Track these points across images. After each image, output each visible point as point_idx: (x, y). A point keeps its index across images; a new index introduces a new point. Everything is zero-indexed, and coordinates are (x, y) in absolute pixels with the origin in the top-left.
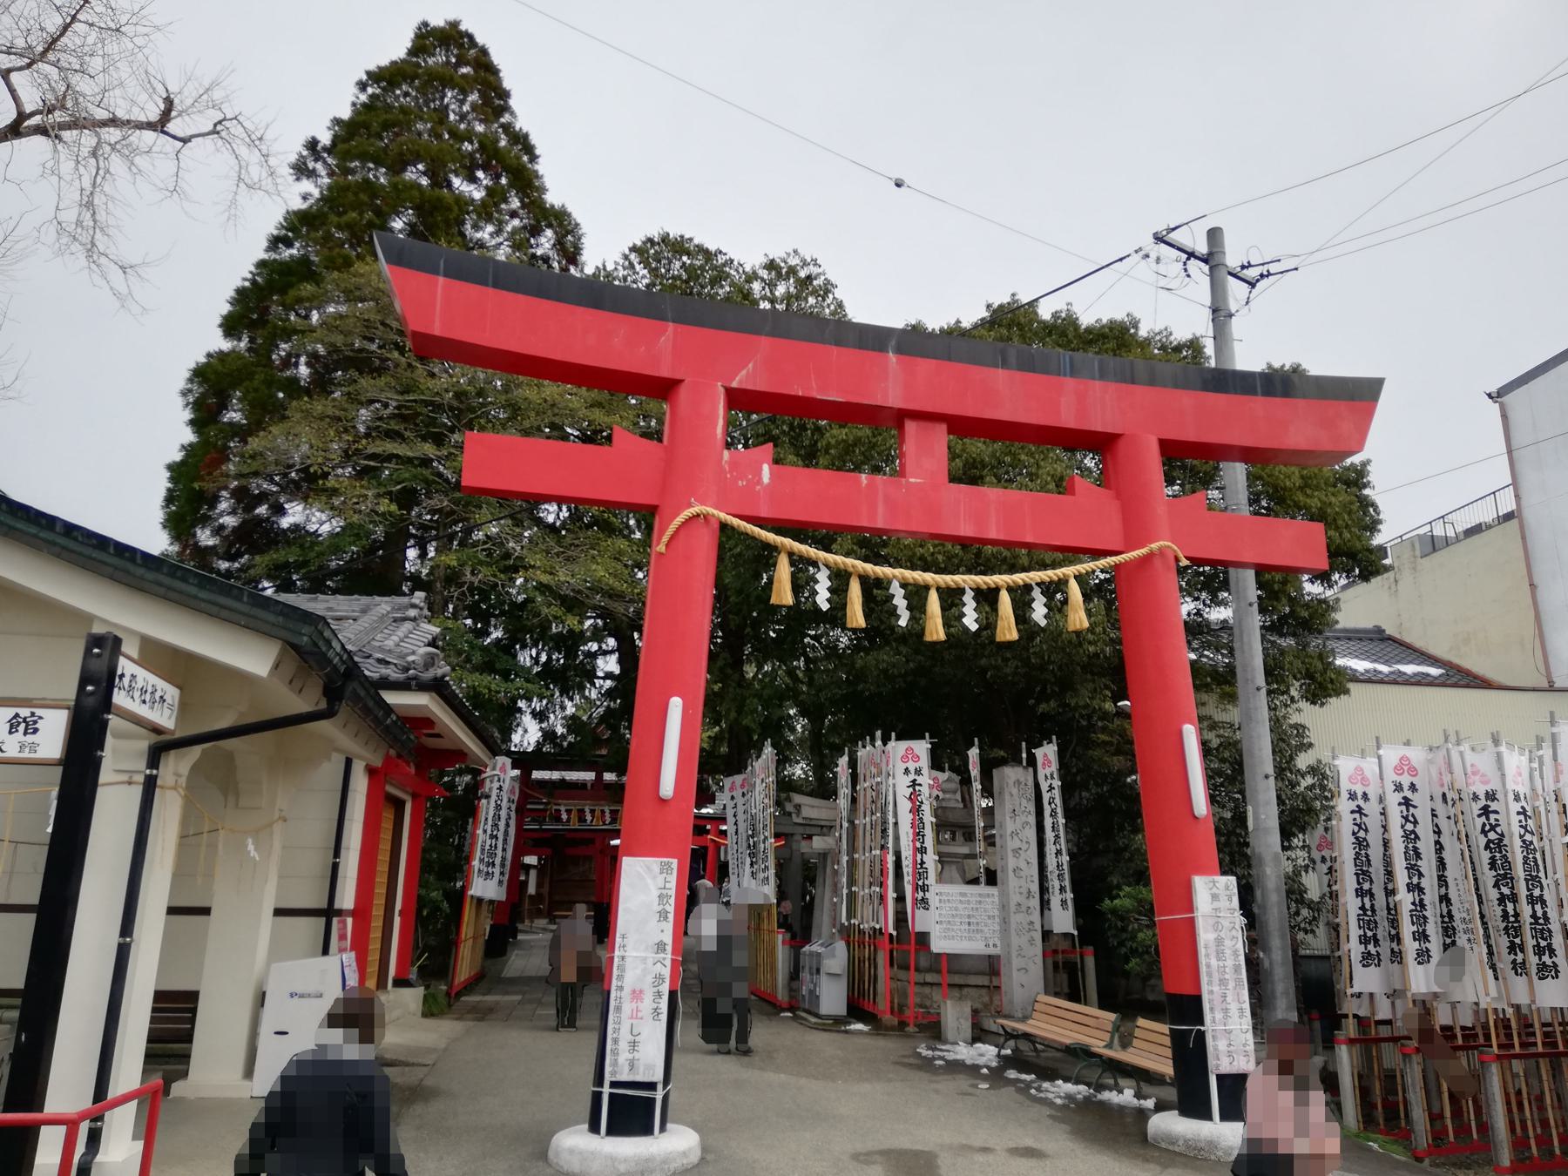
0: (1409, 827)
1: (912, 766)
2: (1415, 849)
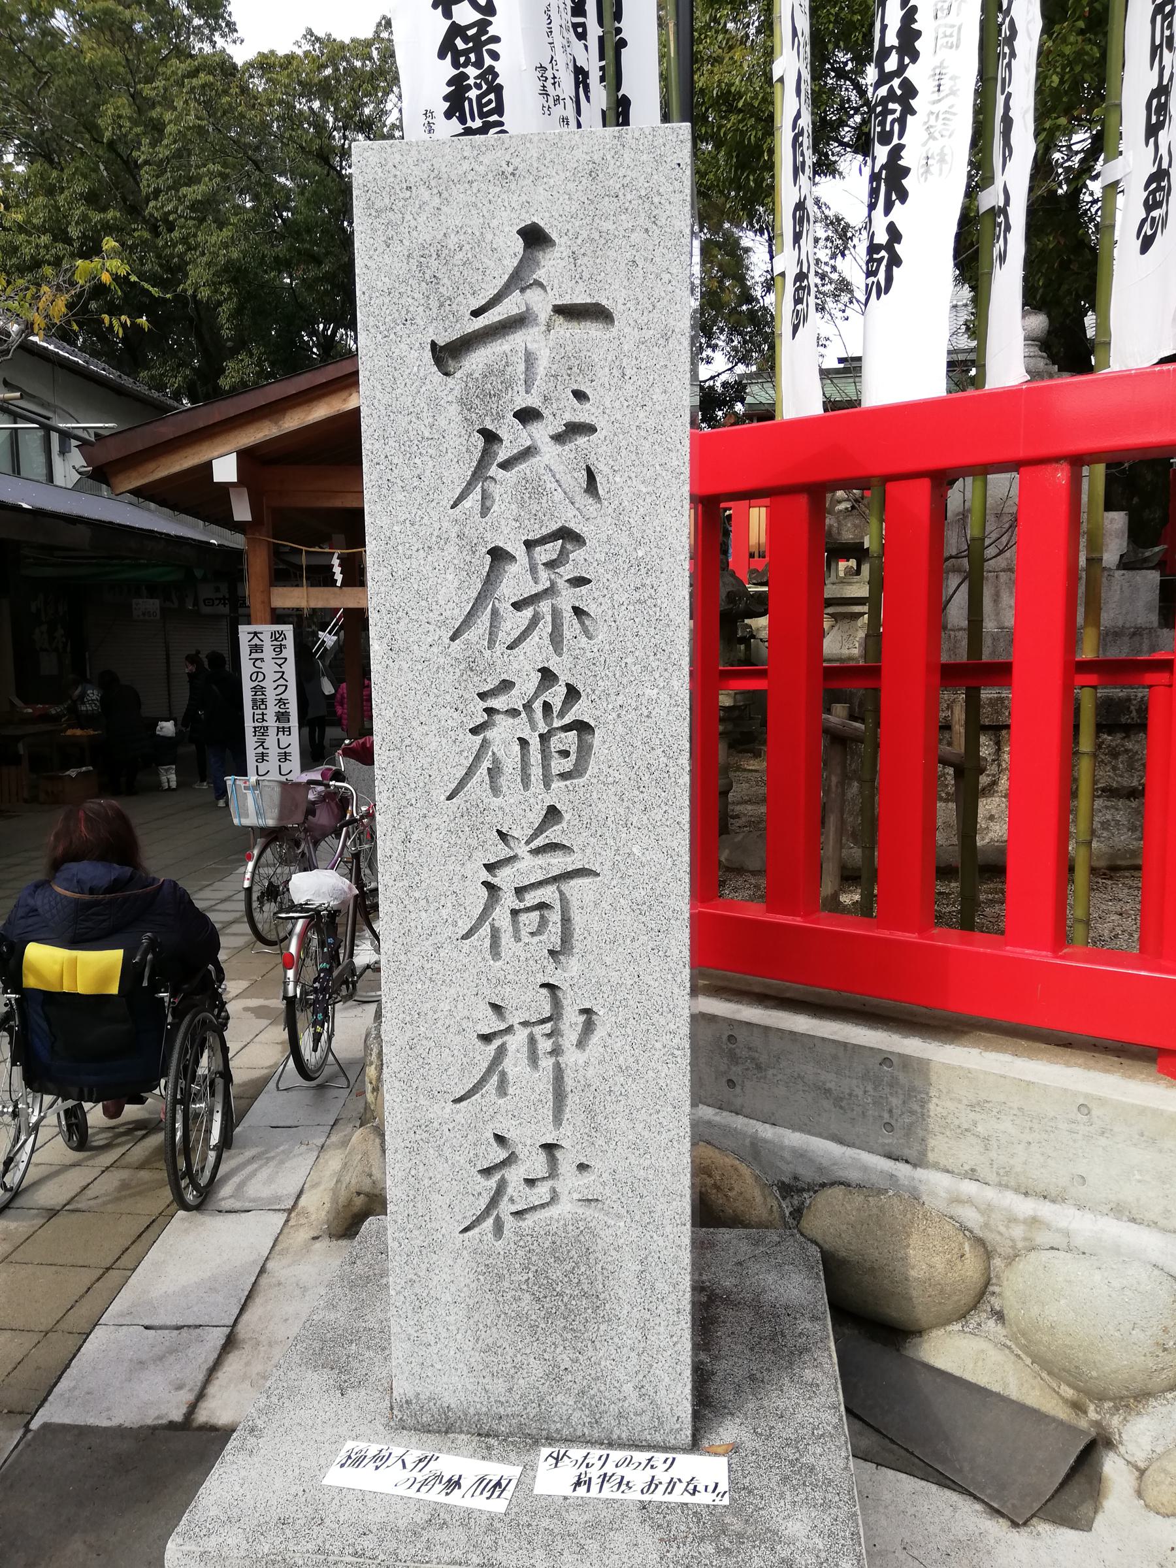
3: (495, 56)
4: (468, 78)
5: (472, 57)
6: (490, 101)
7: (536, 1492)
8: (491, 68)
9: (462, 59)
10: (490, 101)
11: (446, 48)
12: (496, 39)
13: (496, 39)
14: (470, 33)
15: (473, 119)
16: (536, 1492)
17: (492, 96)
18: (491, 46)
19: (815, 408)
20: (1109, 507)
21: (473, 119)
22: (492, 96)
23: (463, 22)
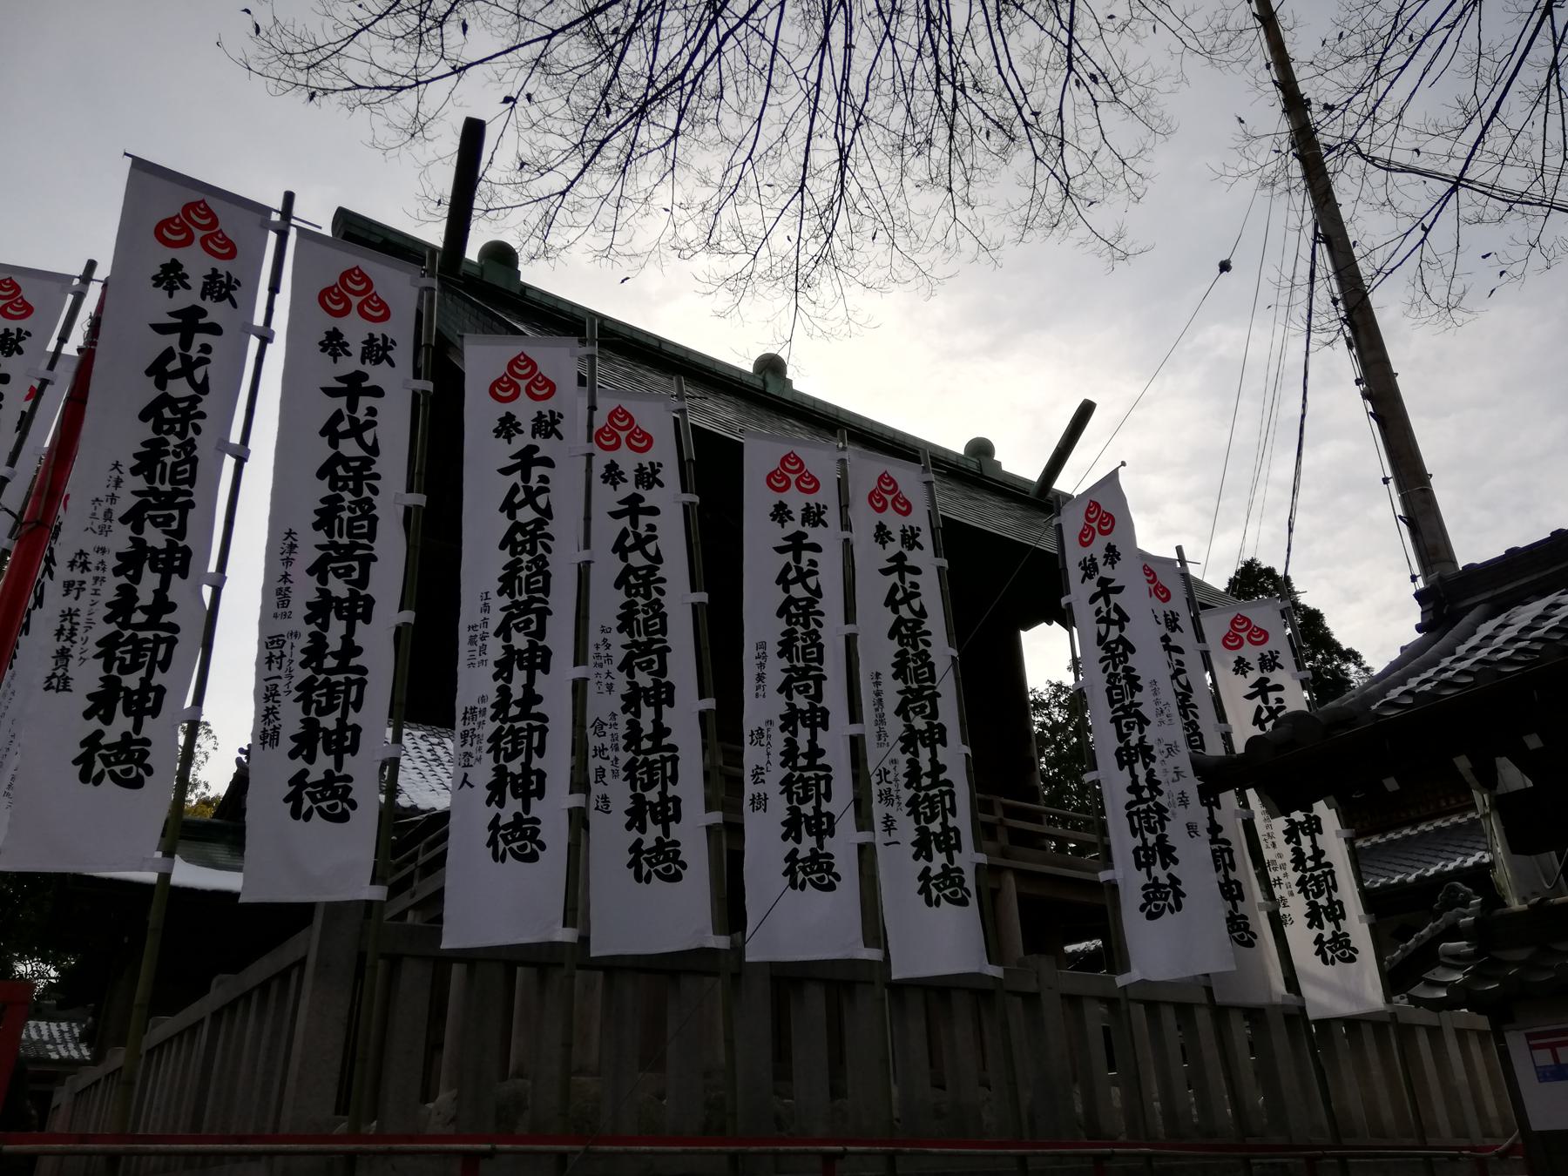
0: (1114, 633)
1: (895, 523)
2: (1128, 670)
3: (198, 430)
4: (167, 444)
5: (178, 427)
6: (185, 471)
7: (450, 940)
8: (192, 440)
9: (166, 427)
10: (185, 471)
11: (508, 541)
12: (202, 415)
13: (202, 415)
14: (181, 405)
15: (162, 482)
16: (450, 940)
17: (365, 523)
18: (197, 421)
19: (1315, 805)
20: (440, 820)
21: (162, 482)
22: (365, 523)
23: (176, 395)
